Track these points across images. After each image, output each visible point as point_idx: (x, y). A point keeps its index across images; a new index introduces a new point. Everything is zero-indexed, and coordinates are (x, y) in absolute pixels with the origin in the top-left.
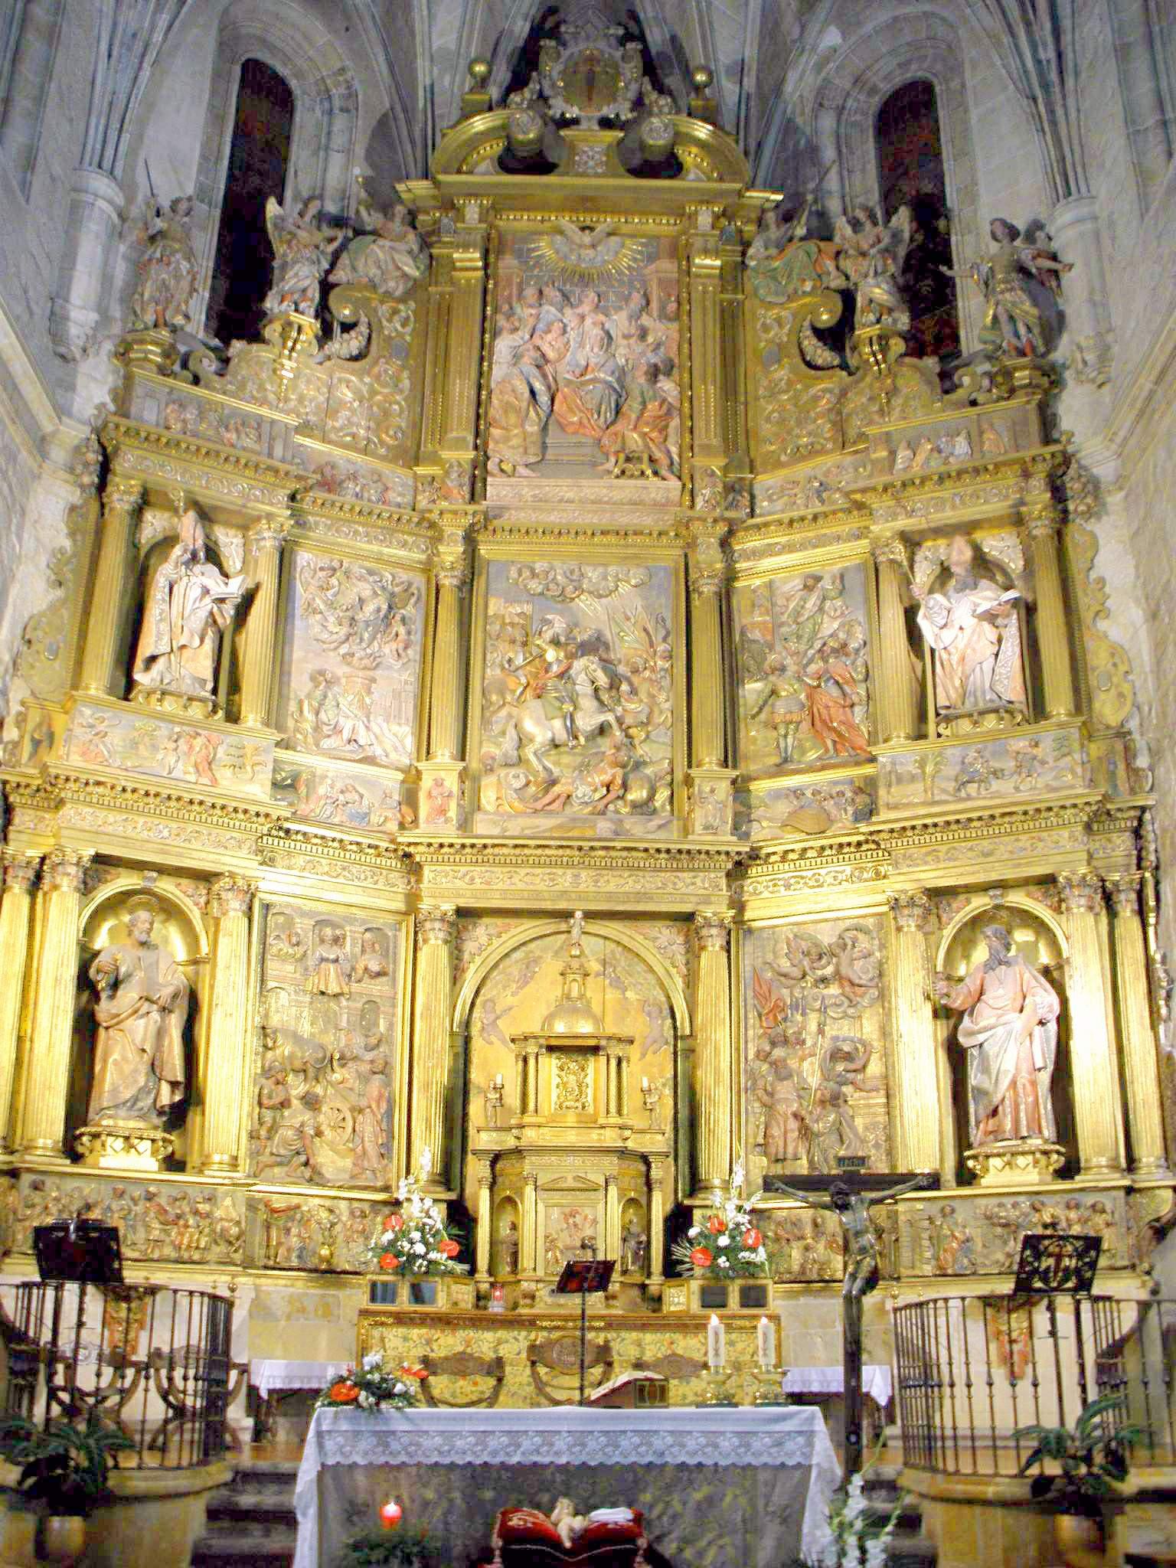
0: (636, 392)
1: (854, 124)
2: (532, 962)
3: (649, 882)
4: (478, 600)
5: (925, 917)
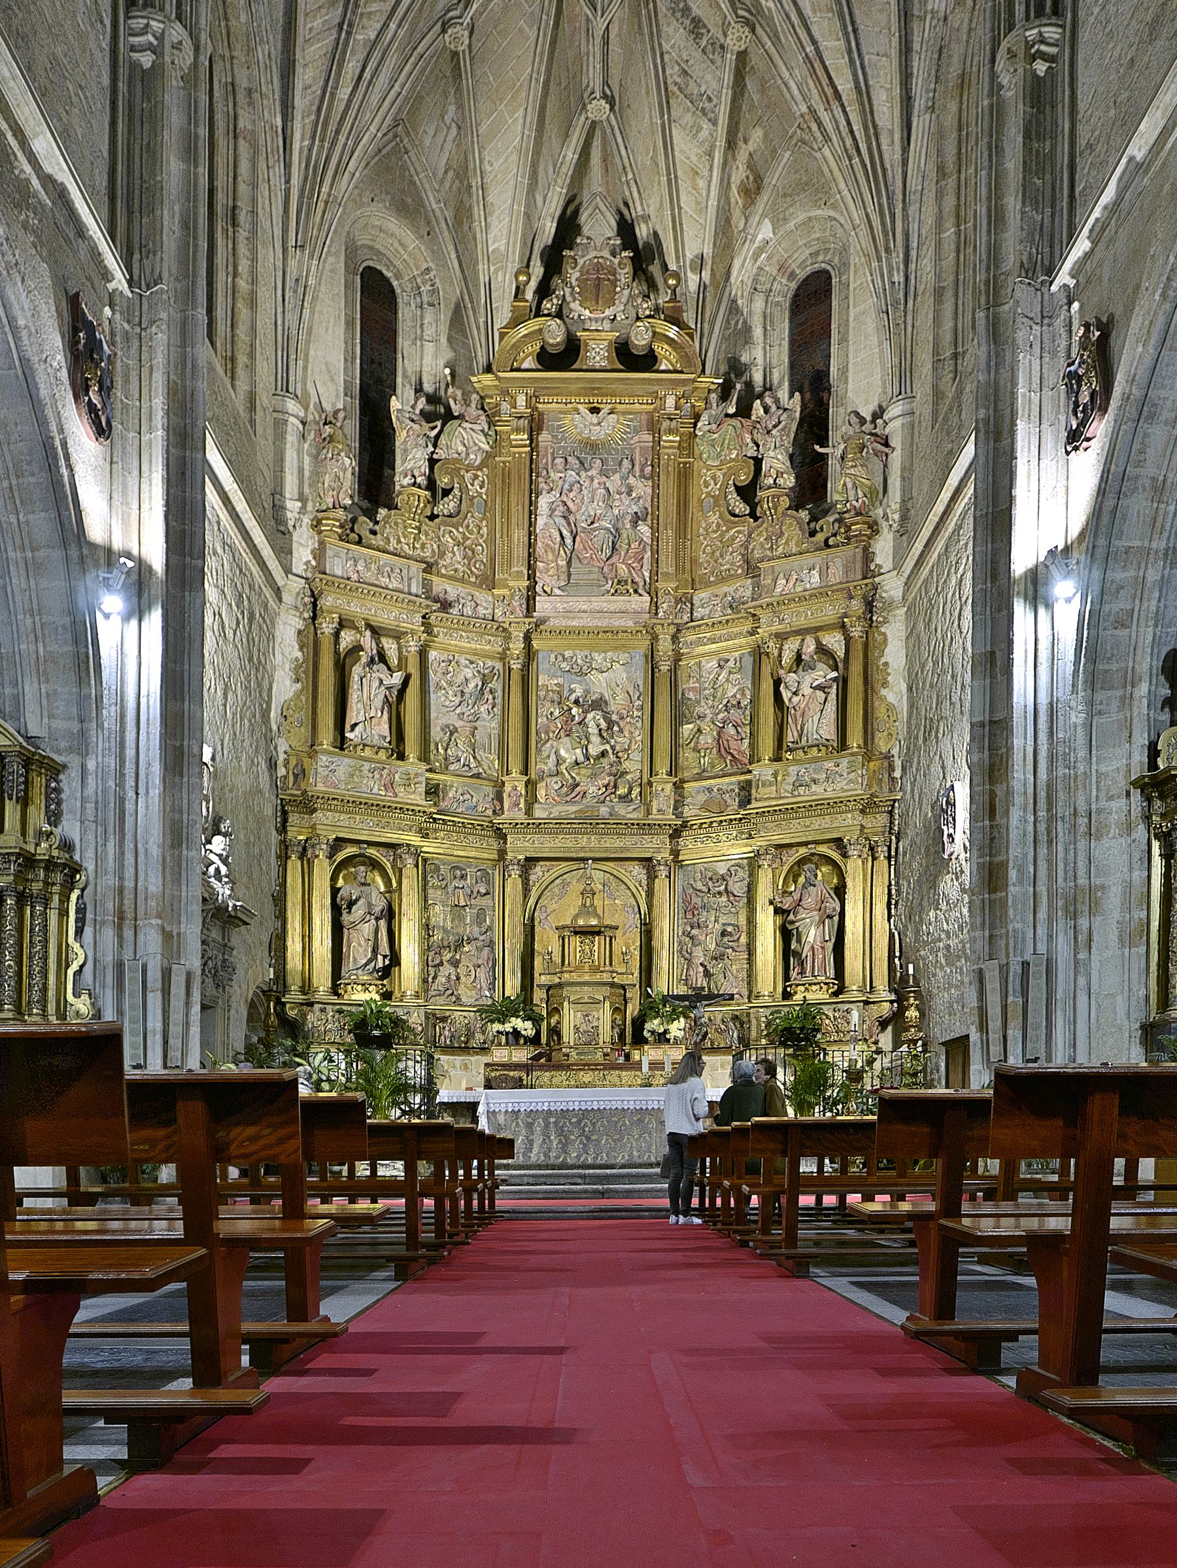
0: (624, 536)
1: (778, 304)
2: (565, 885)
3: (628, 841)
4: (533, 676)
5: (773, 861)
